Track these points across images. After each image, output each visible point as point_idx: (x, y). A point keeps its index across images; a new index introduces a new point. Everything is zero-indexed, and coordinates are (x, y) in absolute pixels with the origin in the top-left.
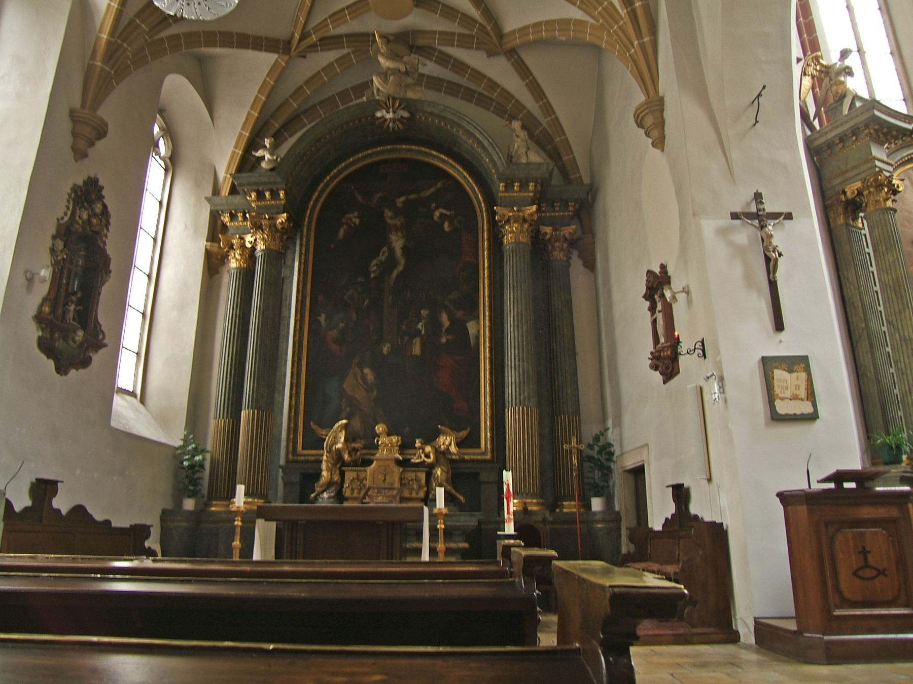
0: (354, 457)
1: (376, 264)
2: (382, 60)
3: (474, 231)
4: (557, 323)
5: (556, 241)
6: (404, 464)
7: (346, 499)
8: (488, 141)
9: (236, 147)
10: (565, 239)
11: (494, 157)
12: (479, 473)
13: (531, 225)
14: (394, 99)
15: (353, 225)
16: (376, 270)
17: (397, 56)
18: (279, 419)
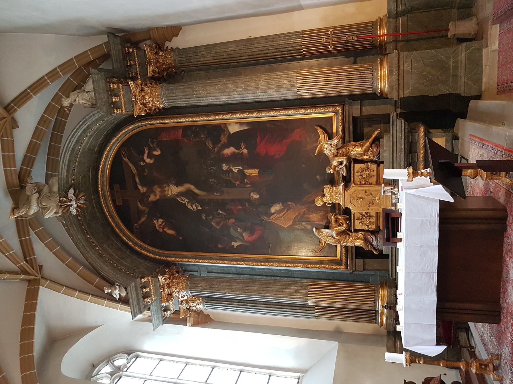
0: (344, 222)
1: (191, 205)
2: (32, 212)
3: (158, 131)
4: (225, 57)
5: (158, 62)
6: (347, 181)
7: (378, 227)
8: (81, 125)
9: (117, 309)
10: (157, 53)
11: (93, 120)
12: (353, 117)
13: (146, 85)
14: (60, 201)
15: (164, 224)
16: (195, 205)
17: (28, 199)
18: (313, 274)
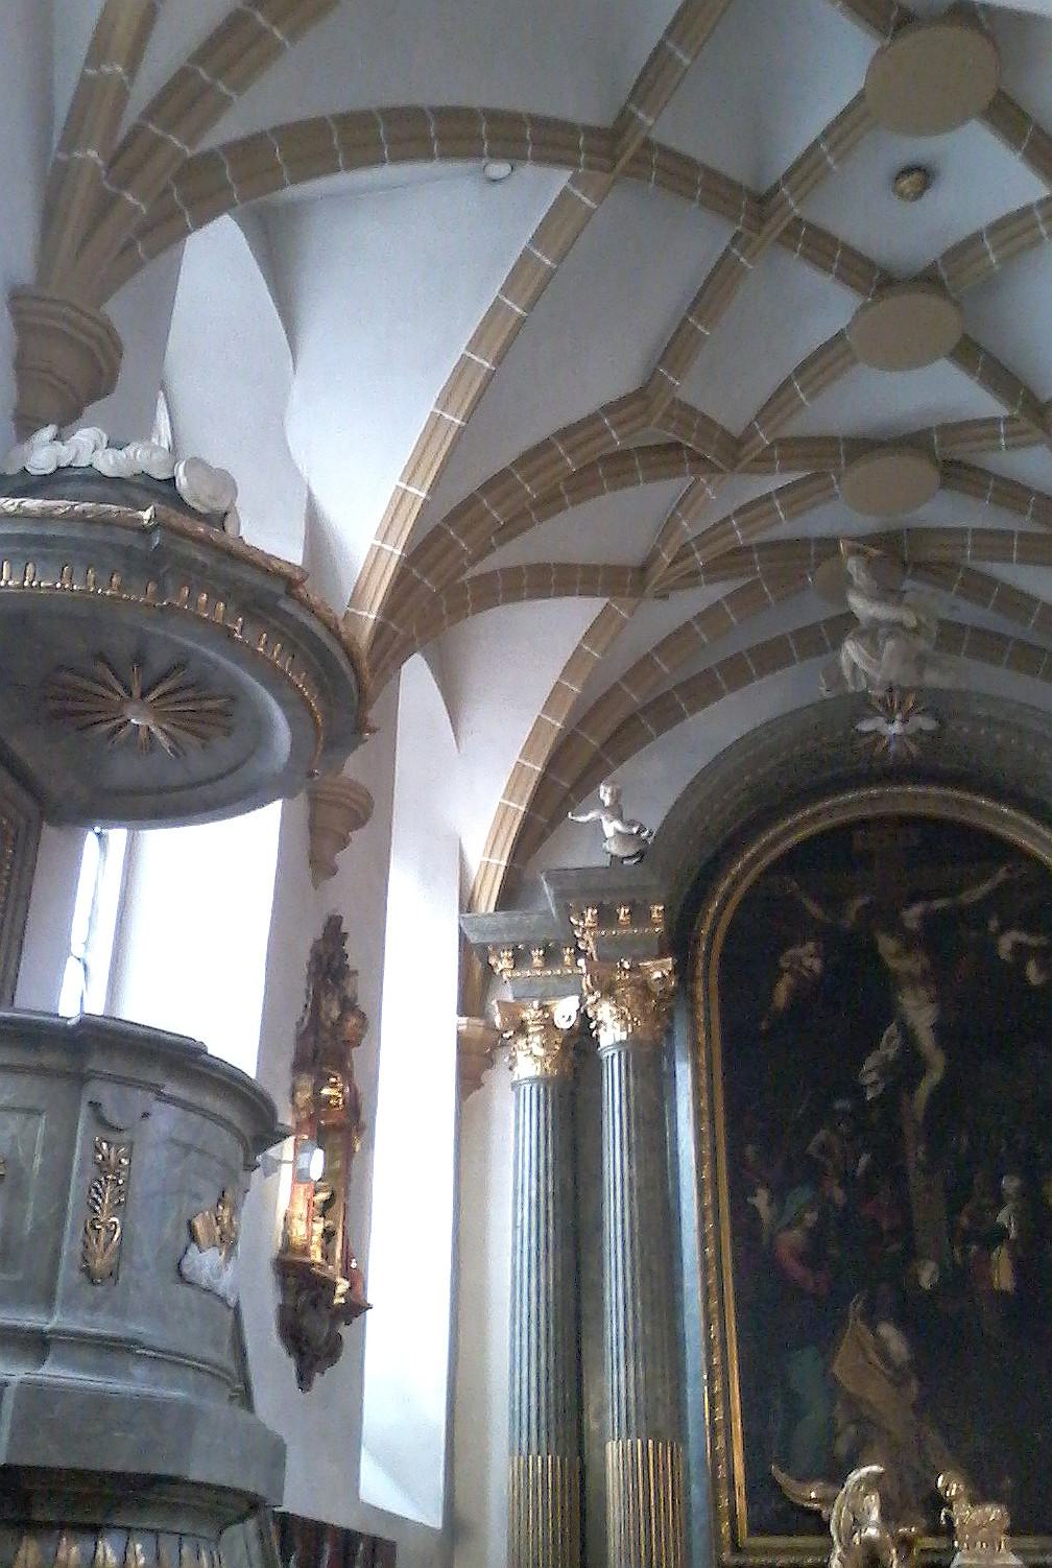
14: (905, 692)
15: (806, 974)
